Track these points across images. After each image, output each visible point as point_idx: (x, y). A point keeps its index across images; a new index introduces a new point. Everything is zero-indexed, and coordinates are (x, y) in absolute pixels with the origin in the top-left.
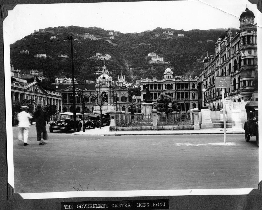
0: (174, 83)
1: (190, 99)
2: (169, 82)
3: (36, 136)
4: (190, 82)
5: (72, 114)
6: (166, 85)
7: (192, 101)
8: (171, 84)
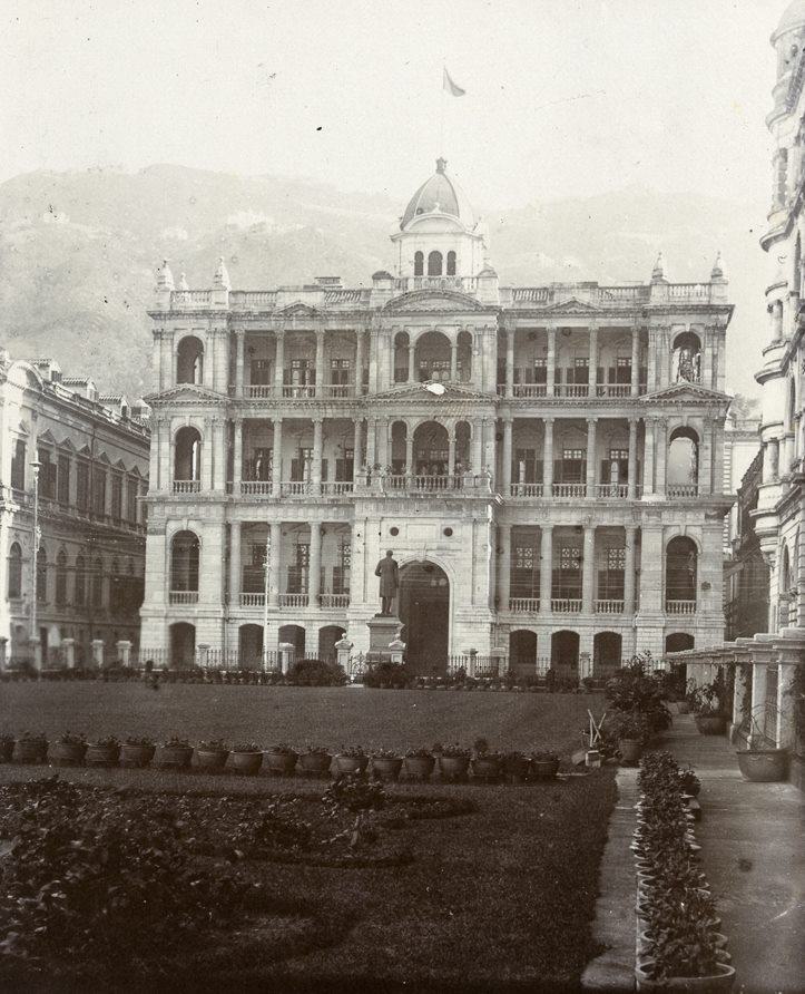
0: (492, 321)
1: (638, 493)
2: (434, 313)
3: (549, 657)
4: (654, 321)
5: (780, 666)
6: (401, 340)
7: (659, 509)
8: (452, 333)
